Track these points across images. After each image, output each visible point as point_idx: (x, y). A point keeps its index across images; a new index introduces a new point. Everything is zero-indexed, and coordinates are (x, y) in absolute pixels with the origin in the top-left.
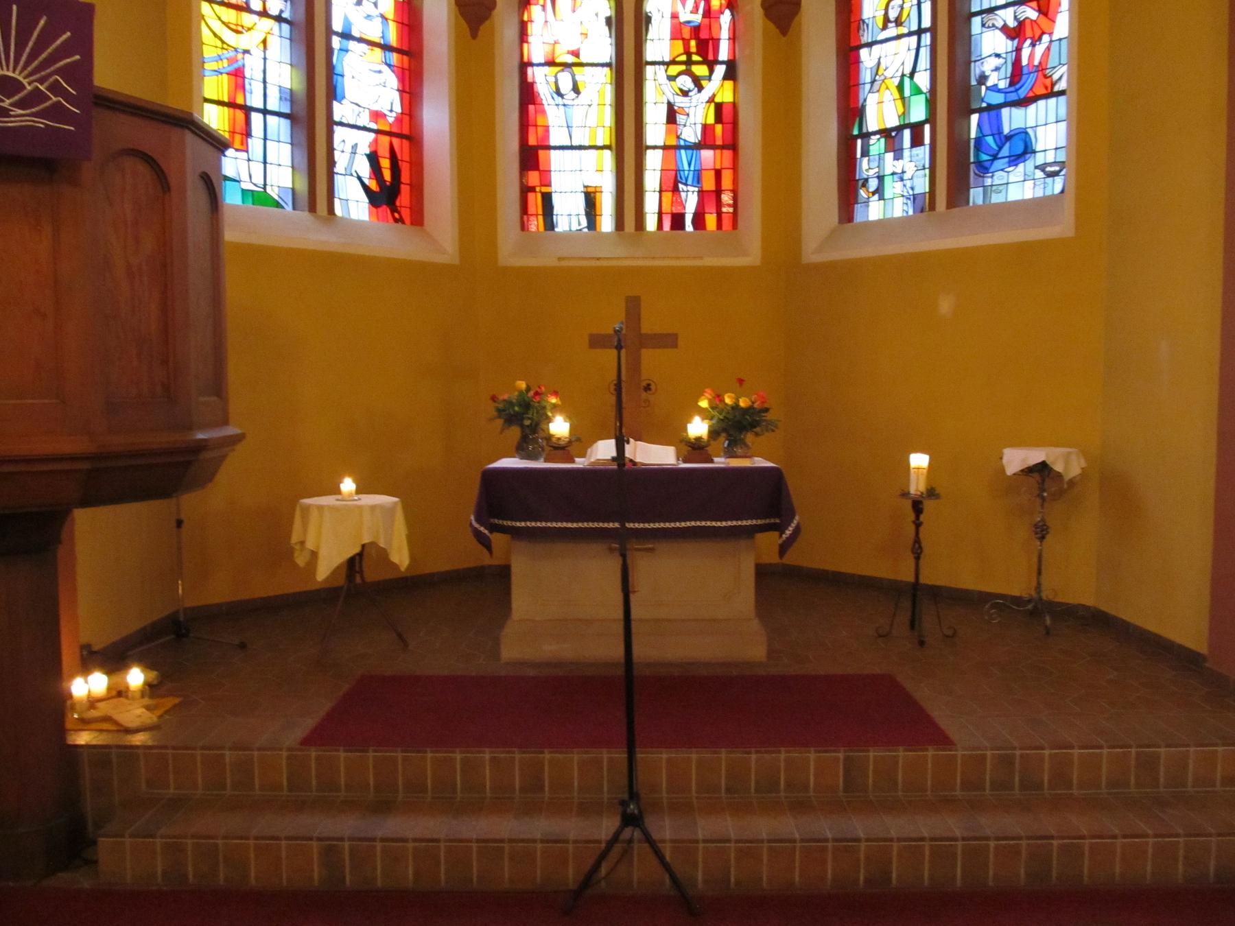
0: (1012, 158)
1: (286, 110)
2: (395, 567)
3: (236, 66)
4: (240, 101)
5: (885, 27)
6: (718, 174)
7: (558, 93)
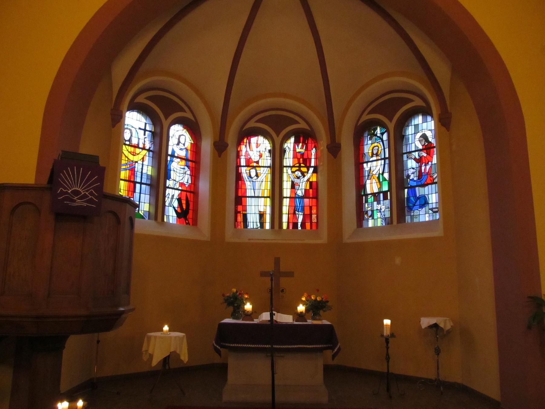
0: (420, 206)
1: (149, 182)
2: (182, 361)
3: (132, 167)
4: (132, 180)
5: (372, 156)
6: (311, 208)
7: (250, 176)
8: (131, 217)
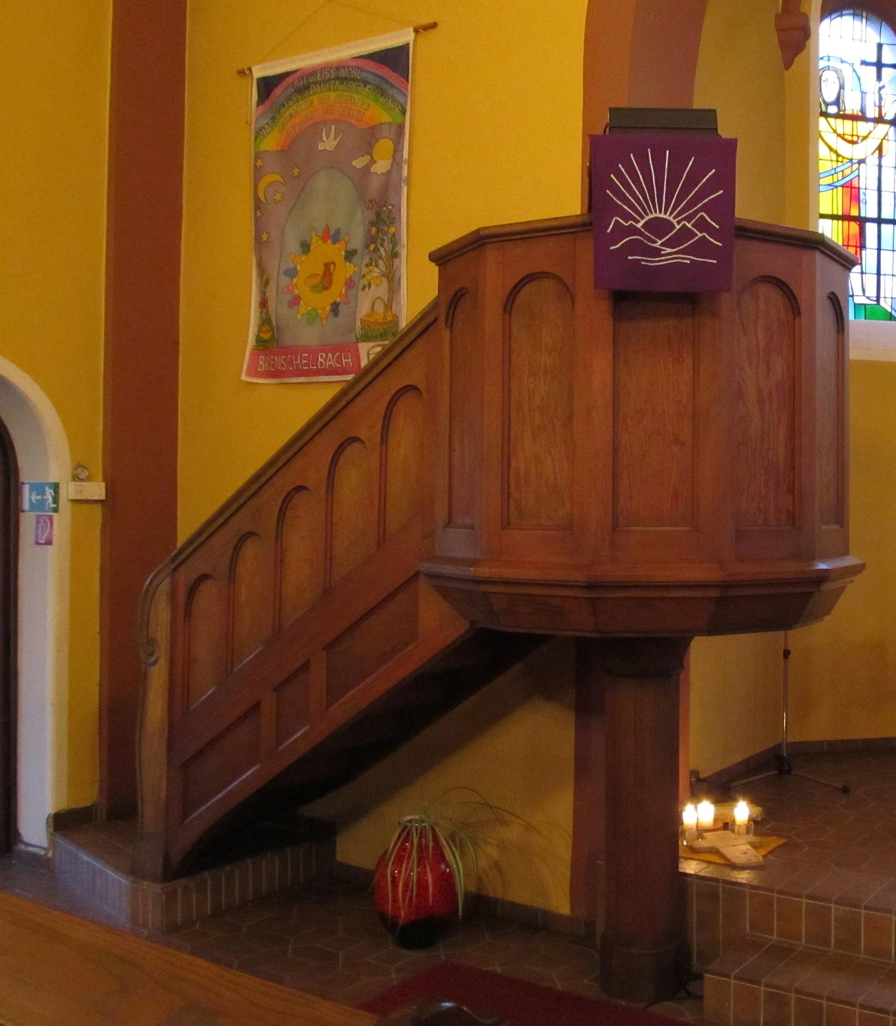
4: (854, 212)
8: (833, 293)
